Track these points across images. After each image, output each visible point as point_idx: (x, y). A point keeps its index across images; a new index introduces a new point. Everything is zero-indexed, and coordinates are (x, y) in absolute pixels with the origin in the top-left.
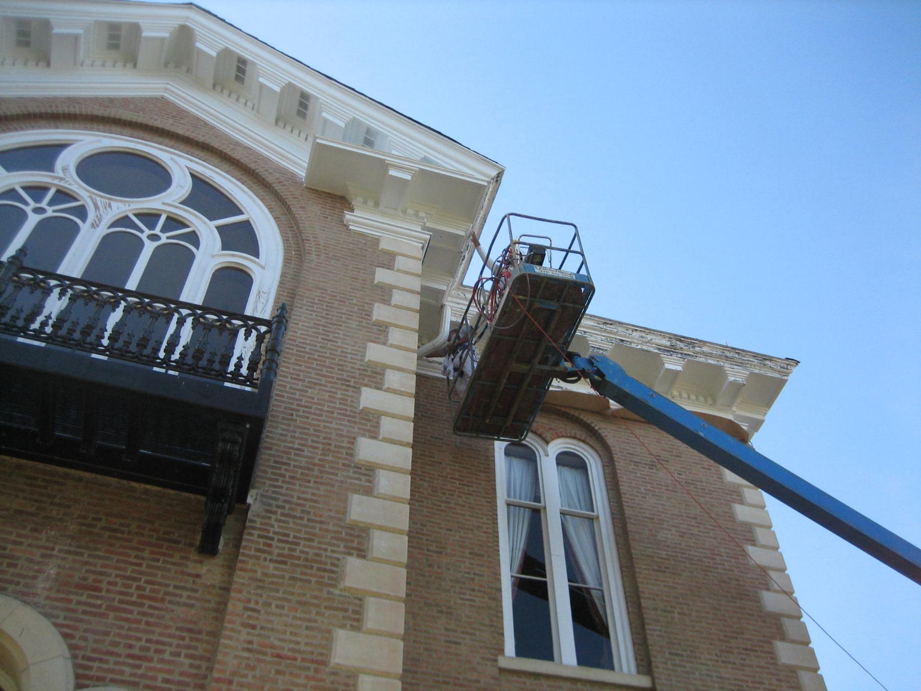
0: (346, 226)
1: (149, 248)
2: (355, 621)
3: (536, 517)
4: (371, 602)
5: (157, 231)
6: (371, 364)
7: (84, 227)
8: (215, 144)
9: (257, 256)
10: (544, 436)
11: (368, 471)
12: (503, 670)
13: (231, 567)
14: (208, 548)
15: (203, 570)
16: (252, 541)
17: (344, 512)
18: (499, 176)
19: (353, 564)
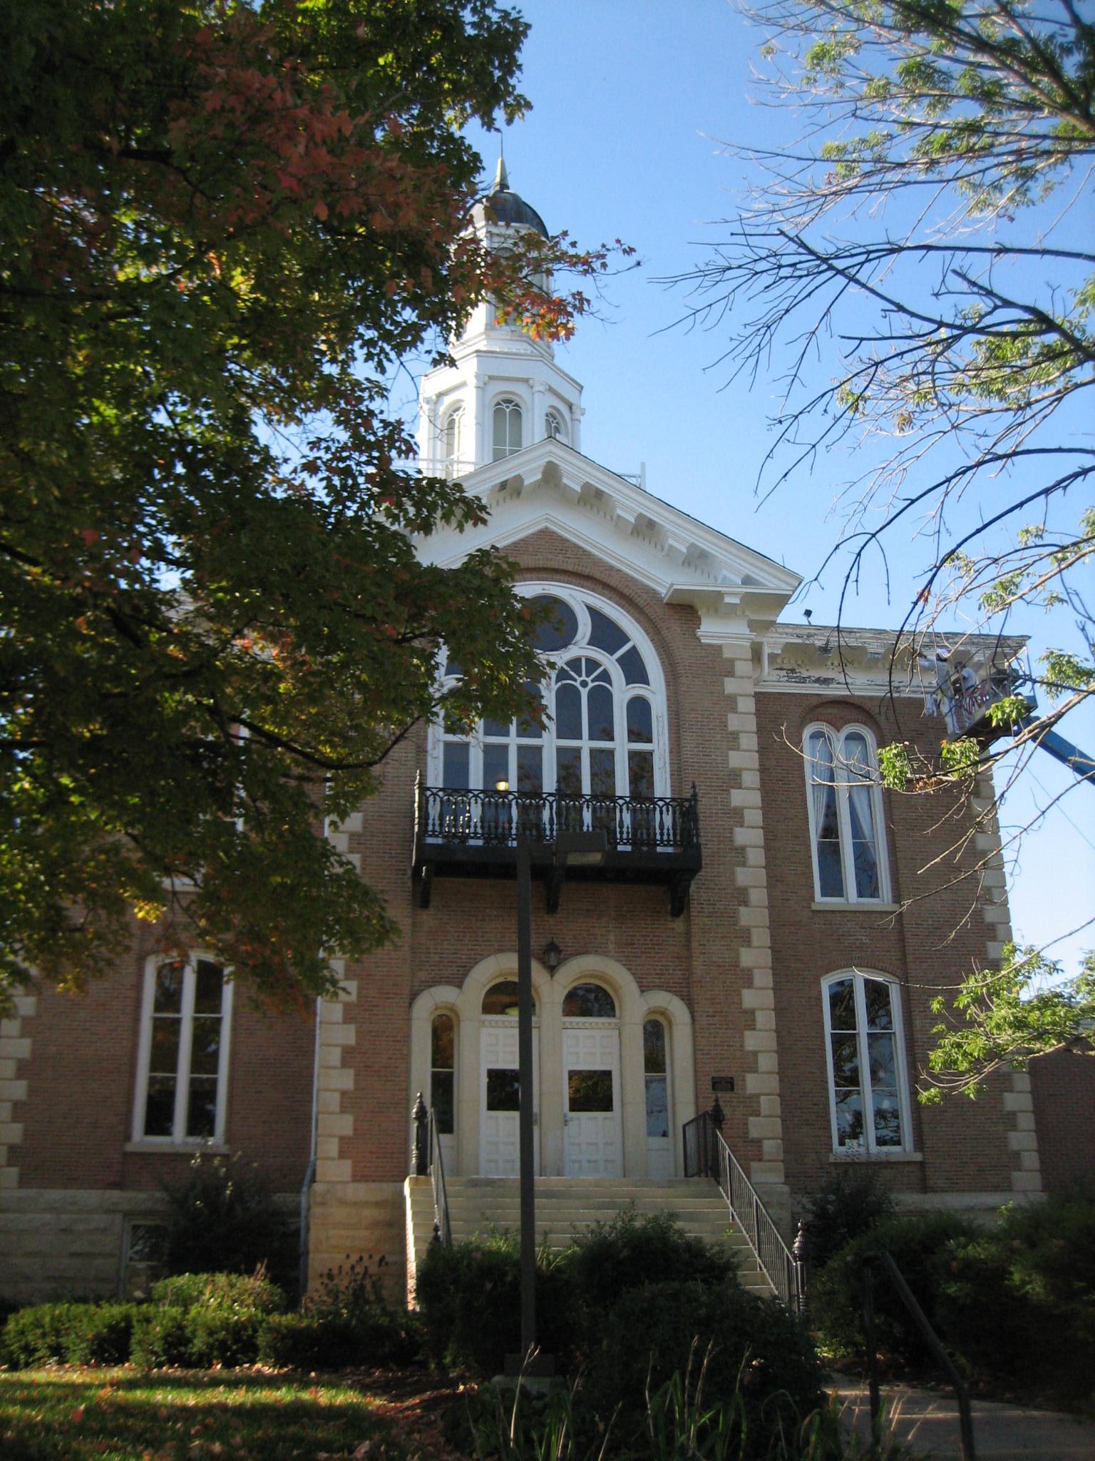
0: (698, 639)
1: (584, 693)
2: (747, 942)
5: (584, 678)
11: (741, 851)
12: (814, 911)
13: (688, 921)
15: (675, 925)
16: (694, 908)
17: (733, 880)
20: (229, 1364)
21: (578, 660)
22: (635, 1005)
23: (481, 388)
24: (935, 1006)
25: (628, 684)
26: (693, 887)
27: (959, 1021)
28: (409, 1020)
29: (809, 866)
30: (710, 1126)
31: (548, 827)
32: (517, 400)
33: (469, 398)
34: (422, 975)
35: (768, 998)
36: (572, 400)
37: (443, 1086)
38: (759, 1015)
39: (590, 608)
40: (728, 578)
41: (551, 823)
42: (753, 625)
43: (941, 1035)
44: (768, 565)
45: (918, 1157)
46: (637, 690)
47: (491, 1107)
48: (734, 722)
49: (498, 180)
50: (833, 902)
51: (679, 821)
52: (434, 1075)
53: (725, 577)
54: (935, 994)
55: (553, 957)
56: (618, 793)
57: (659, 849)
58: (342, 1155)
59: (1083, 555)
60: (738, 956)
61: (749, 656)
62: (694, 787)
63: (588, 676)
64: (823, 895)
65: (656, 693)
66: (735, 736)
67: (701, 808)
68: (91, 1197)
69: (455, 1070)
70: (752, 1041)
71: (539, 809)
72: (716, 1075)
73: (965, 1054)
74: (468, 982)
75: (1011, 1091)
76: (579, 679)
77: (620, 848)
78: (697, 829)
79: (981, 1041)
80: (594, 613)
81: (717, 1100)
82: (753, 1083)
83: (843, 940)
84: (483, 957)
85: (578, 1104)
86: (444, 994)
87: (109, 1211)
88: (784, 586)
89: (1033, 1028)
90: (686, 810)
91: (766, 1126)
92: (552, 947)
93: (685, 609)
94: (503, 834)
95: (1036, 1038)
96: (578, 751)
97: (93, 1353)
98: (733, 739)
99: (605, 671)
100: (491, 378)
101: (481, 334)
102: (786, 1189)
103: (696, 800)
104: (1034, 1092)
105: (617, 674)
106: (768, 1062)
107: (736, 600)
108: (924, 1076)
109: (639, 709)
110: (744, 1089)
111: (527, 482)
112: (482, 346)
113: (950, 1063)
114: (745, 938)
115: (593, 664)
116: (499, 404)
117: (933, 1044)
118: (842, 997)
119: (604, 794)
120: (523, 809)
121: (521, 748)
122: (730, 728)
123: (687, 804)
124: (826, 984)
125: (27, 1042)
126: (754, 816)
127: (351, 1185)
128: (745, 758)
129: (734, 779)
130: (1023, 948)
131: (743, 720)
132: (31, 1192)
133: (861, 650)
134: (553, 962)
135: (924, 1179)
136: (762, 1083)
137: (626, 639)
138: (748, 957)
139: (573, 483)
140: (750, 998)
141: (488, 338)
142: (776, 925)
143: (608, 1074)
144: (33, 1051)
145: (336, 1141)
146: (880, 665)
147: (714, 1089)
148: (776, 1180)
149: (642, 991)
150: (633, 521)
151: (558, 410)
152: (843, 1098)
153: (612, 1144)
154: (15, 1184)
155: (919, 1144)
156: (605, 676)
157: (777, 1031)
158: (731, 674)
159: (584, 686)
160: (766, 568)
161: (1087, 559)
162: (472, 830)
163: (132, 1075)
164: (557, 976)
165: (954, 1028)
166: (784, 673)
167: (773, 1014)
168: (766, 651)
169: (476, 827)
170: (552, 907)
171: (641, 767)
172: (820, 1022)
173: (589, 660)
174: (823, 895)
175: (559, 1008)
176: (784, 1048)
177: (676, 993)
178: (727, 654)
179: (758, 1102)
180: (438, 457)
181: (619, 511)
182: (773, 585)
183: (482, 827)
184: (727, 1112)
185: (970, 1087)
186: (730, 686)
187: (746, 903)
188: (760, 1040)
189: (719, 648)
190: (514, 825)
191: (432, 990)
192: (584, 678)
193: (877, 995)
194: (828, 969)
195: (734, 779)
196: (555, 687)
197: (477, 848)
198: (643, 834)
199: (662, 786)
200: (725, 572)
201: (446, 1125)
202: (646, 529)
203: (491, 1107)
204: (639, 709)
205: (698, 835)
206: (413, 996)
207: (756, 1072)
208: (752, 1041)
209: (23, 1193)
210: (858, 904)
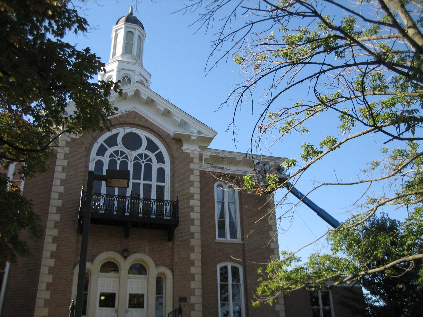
0: (182, 150)
1: (143, 165)
2: (193, 251)
3: (223, 203)
4: (195, 220)
5: (143, 160)
6: (191, 193)
7: (129, 162)
8: (150, 127)
11: (193, 220)
12: (216, 243)
13: (173, 243)
16: (176, 238)
22: (153, 271)
23: (118, 72)
24: (259, 271)
25: (157, 163)
26: (175, 232)
27: (266, 277)
29: (215, 228)
30: (177, 314)
32: (130, 76)
35: (199, 270)
36: (147, 79)
40: (193, 131)
41: (128, 207)
42: (200, 147)
43: (261, 282)
44: (207, 128)
46: (161, 165)
48: (192, 178)
49: (130, 12)
50: (222, 240)
51: (172, 209)
53: (192, 131)
54: (259, 266)
56: (152, 198)
57: (165, 218)
59: (317, 112)
61: (198, 157)
62: (178, 197)
63: (144, 159)
64: (219, 237)
65: (167, 167)
66: (192, 182)
67: (180, 205)
69: (88, 292)
72: (181, 296)
73: (269, 289)
77: (152, 216)
78: (178, 211)
79: (275, 284)
80: (148, 139)
81: (180, 305)
82: (193, 299)
83: (223, 252)
84: (101, 252)
85: (103, 304)
88: (212, 135)
89: (293, 279)
90: (175, 205)
92: (126, 250)
93: (178, 140)
95: (293, 284)
98: (192, 183)
99: (150, 158)
101: (120, 56)
103: (178, 202)
105: (154, 160)
106: (198, 292)
107: (195, 138)
108: (254, 297)
110: (190, 301)
111: (129, 95)
112: (120, 59)
113: (264, 292)
115: (146, 156)
116: (124, 77)
117: (258, 284)
118: (224, 270)
119: (147, 198)
122: (191, 180)
123: (175, 203)
124: (219, 267)
126: (197, 209)
128: (195, 190)
129: (191, 196)
130: (288, 253)
131: (195, 178)
133: (234, 159)
136: (196, 299)
137: (158, 148)
138: (193, 256)
139: (144, 96)
140: (193, 270)
141: (122, 57)
142: (203, 246)
143: (143, 296)
146: (240, 164)
152: (223, 305)
156: (150, 160)
157: (202, 282)
158: (192, 162)
159: (143, 163)
160: (206, 129)
161: (318, 114)
162: (100, 207)
164: (127, 260)
165: (266, 279)
166: (209, 165)
167: (201, 276)
168: (204, 157)
169: (101, 206)
170: (127, 236)
171: (160, 189)
172: (216, 280)
174: (219, 237)
175: (127, 271)
176: (204, 288)
178: (191, 156)
179: (194, 306)
181: (159, 107)
182: (207, 134)
183: (104, 207)
184: (183, 309)
185: (270, 301)
186: (192, 166)
188: (196, 285)
189: (189, 154)
192: (143, 160)
193: (235, 271)
194: (220, 262)
195: (191, 196)
196: (133, 163)
197: (102, 214)
198: (160, 212)
199: (167, 197)
200: (192, 129)
202: (167, 113)
204: (161, 172)
205: (178, 214)
207: (194, 295)
208: (193, 285)
210: (230, 241)
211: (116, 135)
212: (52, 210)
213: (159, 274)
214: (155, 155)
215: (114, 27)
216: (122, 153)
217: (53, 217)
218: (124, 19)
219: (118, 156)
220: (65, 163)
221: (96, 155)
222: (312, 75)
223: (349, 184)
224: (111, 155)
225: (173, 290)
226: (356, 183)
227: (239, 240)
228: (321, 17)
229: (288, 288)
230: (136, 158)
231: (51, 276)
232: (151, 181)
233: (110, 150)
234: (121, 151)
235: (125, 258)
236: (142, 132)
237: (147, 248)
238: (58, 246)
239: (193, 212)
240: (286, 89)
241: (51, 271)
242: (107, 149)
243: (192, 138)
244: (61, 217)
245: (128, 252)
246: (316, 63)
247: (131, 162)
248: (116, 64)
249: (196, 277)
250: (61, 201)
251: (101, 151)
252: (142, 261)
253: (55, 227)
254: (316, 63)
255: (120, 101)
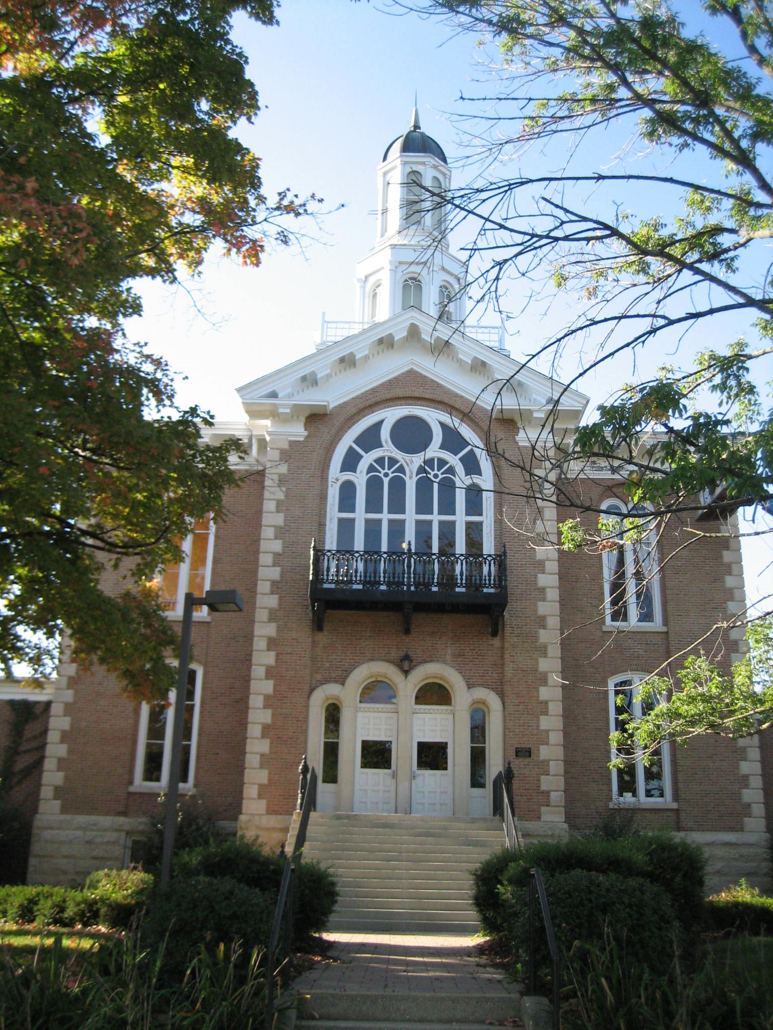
1: (386, 481)
2: (545, 654)
4: (548, 590)
5: (386, 471)
7: (407, 479)
9: (481, 475)
10: (691, 190)
11: (543, 590)
13: (503, 639)
14: (494, 634)
16: (508, 630)
17: (536, 611)
18: (588, 402)
19: (542, 632)
20: (85, 925)
21: (432, 460)
22: (463, 697)
23: (394, 271)
28: (307, 706)
31: (459, 577)
33: (385, 277)
34: (319, 677)
35: (254, 685)
37: (331, 751)
38: (551, 705)
39: (441, 424)
45: (675, 806)
47: (365, 765)
49: (412, 124)
52: (326, 744)
55: (406, 664)
58: (260, 796)
60: (537, 663)
63: (438, 470)
65: (486, 480)
68: (105, 821)
70: (545, 723)
71: (453, 564)
72: (519, 746)
74: (349, 681)
75: (746, 760)
76: (383, 472)
77: (457, 590)
82: (544, 752)
86: (332, 690)
87: (118, 831)
90: (501, 559)
91: (553, 782)
92: (407, 658)
93: (509, 422)
94: (429, 582)
96: (430, 523)
97: (20, 916)
100: (400, 263)
102: (566, 826)
104: (763, 761)
105: (460, 469)
106: (556, 738)
109: (474, 493)
111: (396, 339)
114: (272, 643)
115: (442, 462)
116: (406, 281)
120: (442, 564)
121: (391, 522)
125: (68, 720)
127: (265, 817)
132: (68, 817)
134: (406, 667)
135: (678, 822)
138: (544, 665)
144: (72, 725)
145: (256, 786)
147: (517, 756)
148: (560, 820)
149: (469, 688)
150: (470, 362)
151: (447, 282)
153: (445, 792)
154: (58, 812)
155: (676, 797)
156: (451, 470)
159: (436, 475)
163: (135, 742)
164: (409, 677)
170: (407, 631)
171: (474, 531)
173: (376, 461)
177: (493, 689)
179: (548, 765)
180: (366, 320)
187: (544, 627)
188: (552, 722)
190: (436, 576)
191: (324, 686)
196: (415, 479)
199: (489, 547)
201: (331, 776)
203: (365, 765)
205: (506, 580)
206: (312, 690)
207: (547, 744)
208: (545, 723)
209: (63, 817)
210: (637, 626)
211: (378, 425)
212: (263, 587)
213: (475, 702)
214: (460, 459)
215: (378, 168)
216: (393, 461)
217: (266, 601)
218: (398, 145)
219: (384, 469)
220: (281, 496)
221: (341, 471)
222: (630, 341)
223: (749, 535)
224: (371, 469)
225: (505, 735)
226: (763, 533)
227: (657, 624)
228: (621, 236)
229: (682, 733)
230: (421, 470)
231: (269, 712)
232: (454, 514)
233: (368, 459)
234: (389, 458)
235: (406, 673)
236: (431, 413)
237: (449, 651)
238: (277, 656)
239: (543, 573)
240: (581, 375)
241: (268, 702)
242: (362, 457)
243: (535, 415)
244: (280, 599)
245: (412, 661)
246: (638, 316)
247: (411, 478)
248: (388, 254)
249: (551, 706)
250: (278, 569)
251: (351, 461)
252: (441, 679)
253: (271, 619)
254: (638, 316)
255: (376, 355)
